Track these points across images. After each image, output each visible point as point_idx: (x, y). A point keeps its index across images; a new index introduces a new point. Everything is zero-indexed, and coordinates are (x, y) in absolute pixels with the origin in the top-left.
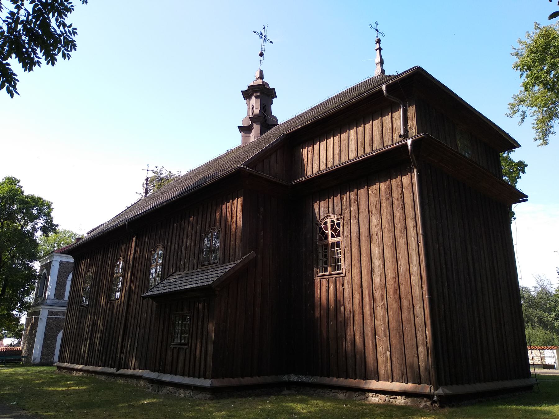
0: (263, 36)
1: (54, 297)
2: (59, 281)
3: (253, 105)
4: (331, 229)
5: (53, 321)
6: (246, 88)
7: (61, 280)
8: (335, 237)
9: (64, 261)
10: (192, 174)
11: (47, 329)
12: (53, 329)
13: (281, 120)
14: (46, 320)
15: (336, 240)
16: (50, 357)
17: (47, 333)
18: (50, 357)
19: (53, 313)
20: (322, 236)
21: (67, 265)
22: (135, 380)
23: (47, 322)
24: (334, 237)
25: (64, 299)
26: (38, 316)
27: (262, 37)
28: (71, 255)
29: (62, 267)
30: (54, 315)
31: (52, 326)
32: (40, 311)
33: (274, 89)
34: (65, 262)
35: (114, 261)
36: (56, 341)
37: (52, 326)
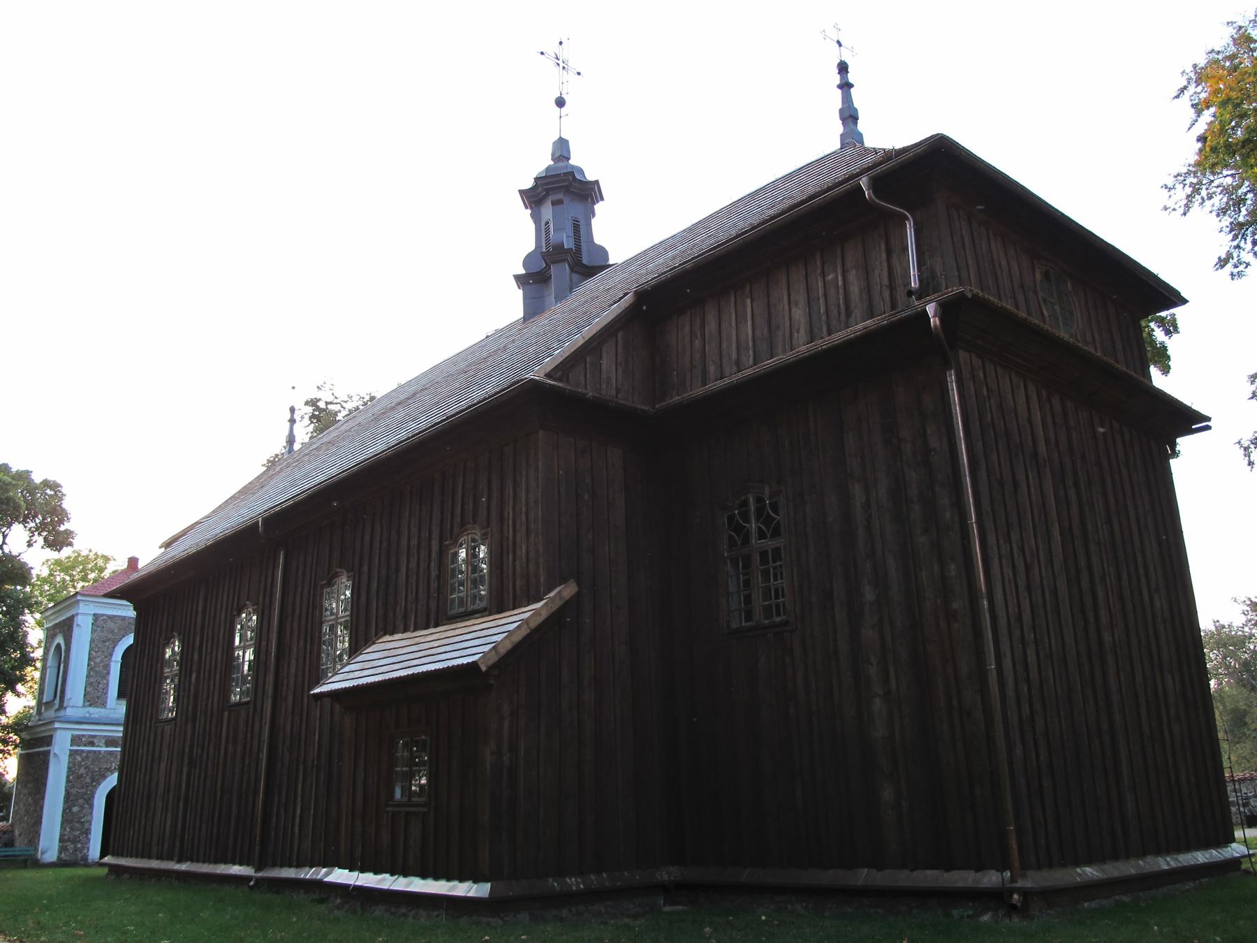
0: (560, 62)
1: (84, 702)
2: (92, 663)
3: (547, 223)
4: (757, 520)
5: (83, 760)
6: (528, 184)
7: (98, 660)
8: (769, 536)
9: (103, 615)
10: (406, 397)
11: (71, 778)
12: (85, 778)
13: (617, 255)
14: (67, 757)
15: (769, 544)
16: (79, 845)
17: (71, 788)
18: (79, 845)
19: (84, 739)
20: (735, 536)
21: (111, 625)
22: (302, 891)
23: (69, 762)
24: (766, 538)
25: (105, 707)
26: (48, 748)
27: (559, 65)
28: (128, 601)
29: (99, 629)
30: (85, 745)
31: (82, 771)
32: (51, 737)
33: (597, 182)
34: (105, 617)
35: (232, 612)
36: (91, 807)
37: (82, 771)
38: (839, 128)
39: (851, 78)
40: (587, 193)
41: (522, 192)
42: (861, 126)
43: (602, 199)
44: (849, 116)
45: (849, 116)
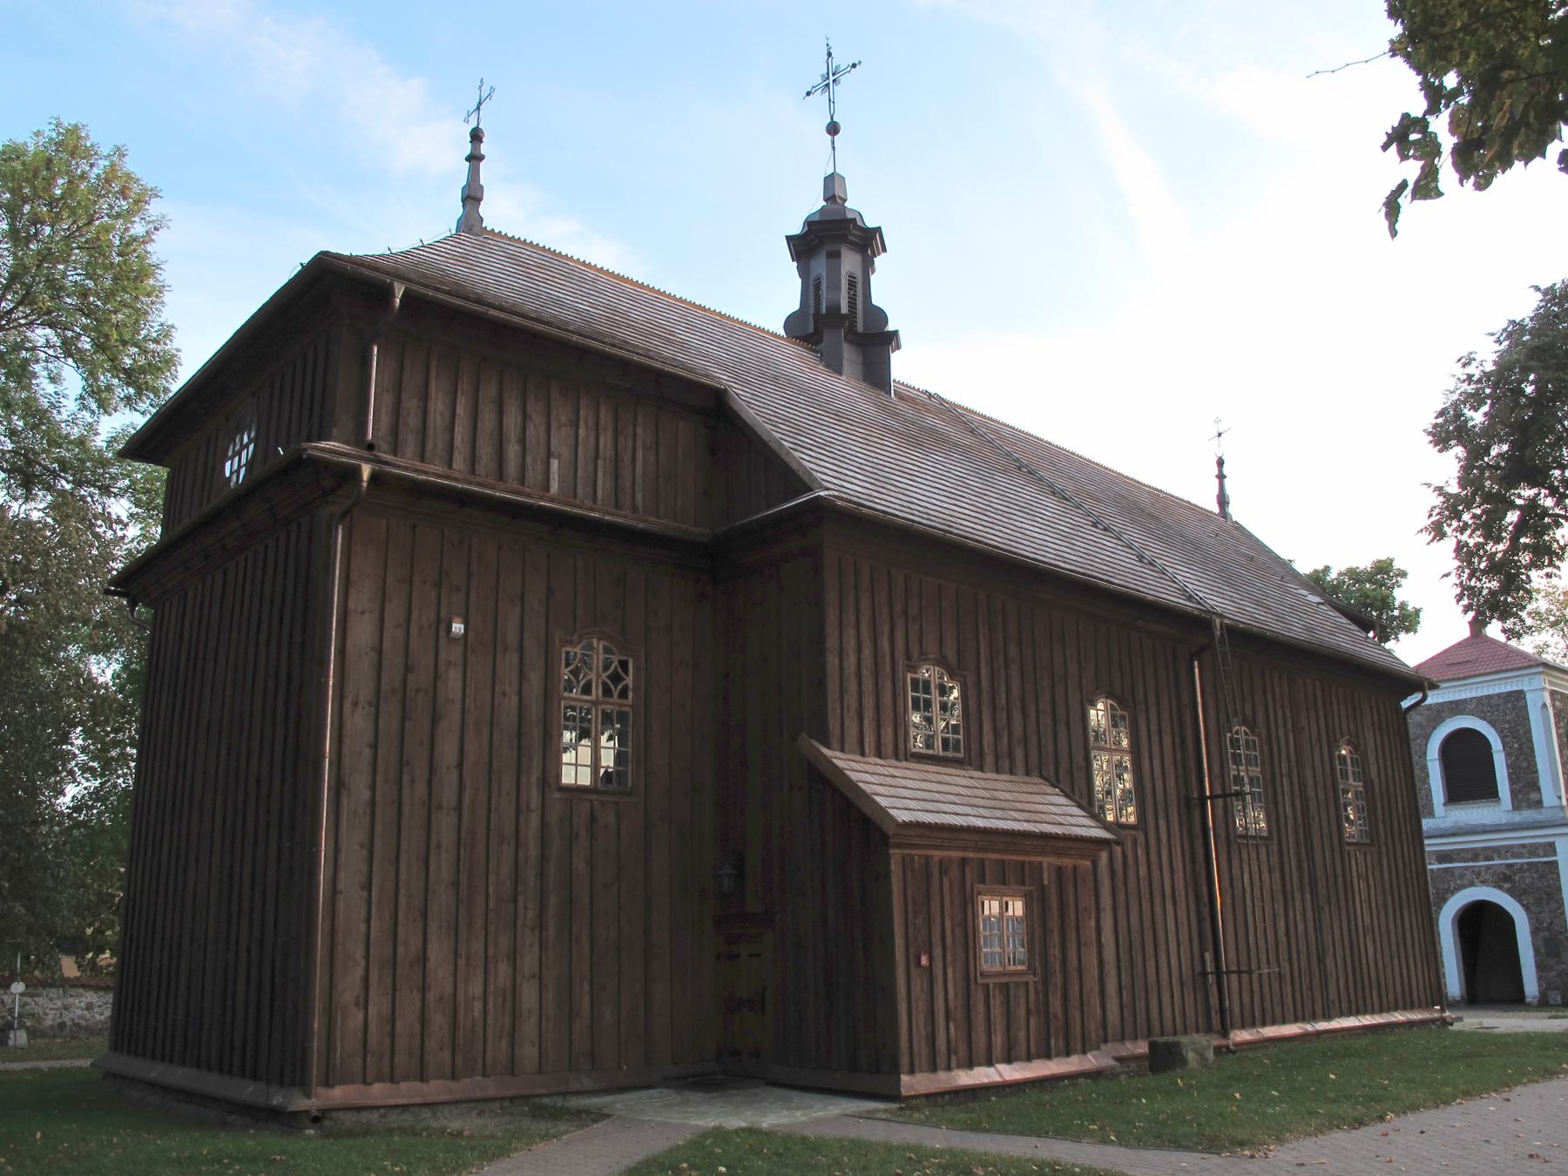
6: (796, 229)
27: (834, 81)
33: (878, 230)
38: (459, 210)
39: (484, 149)
40: (868, 242)
41: (789, 239)
42: (483, 209)
43: (884, 250)
44: (472, 197)
45: (472, 197)
